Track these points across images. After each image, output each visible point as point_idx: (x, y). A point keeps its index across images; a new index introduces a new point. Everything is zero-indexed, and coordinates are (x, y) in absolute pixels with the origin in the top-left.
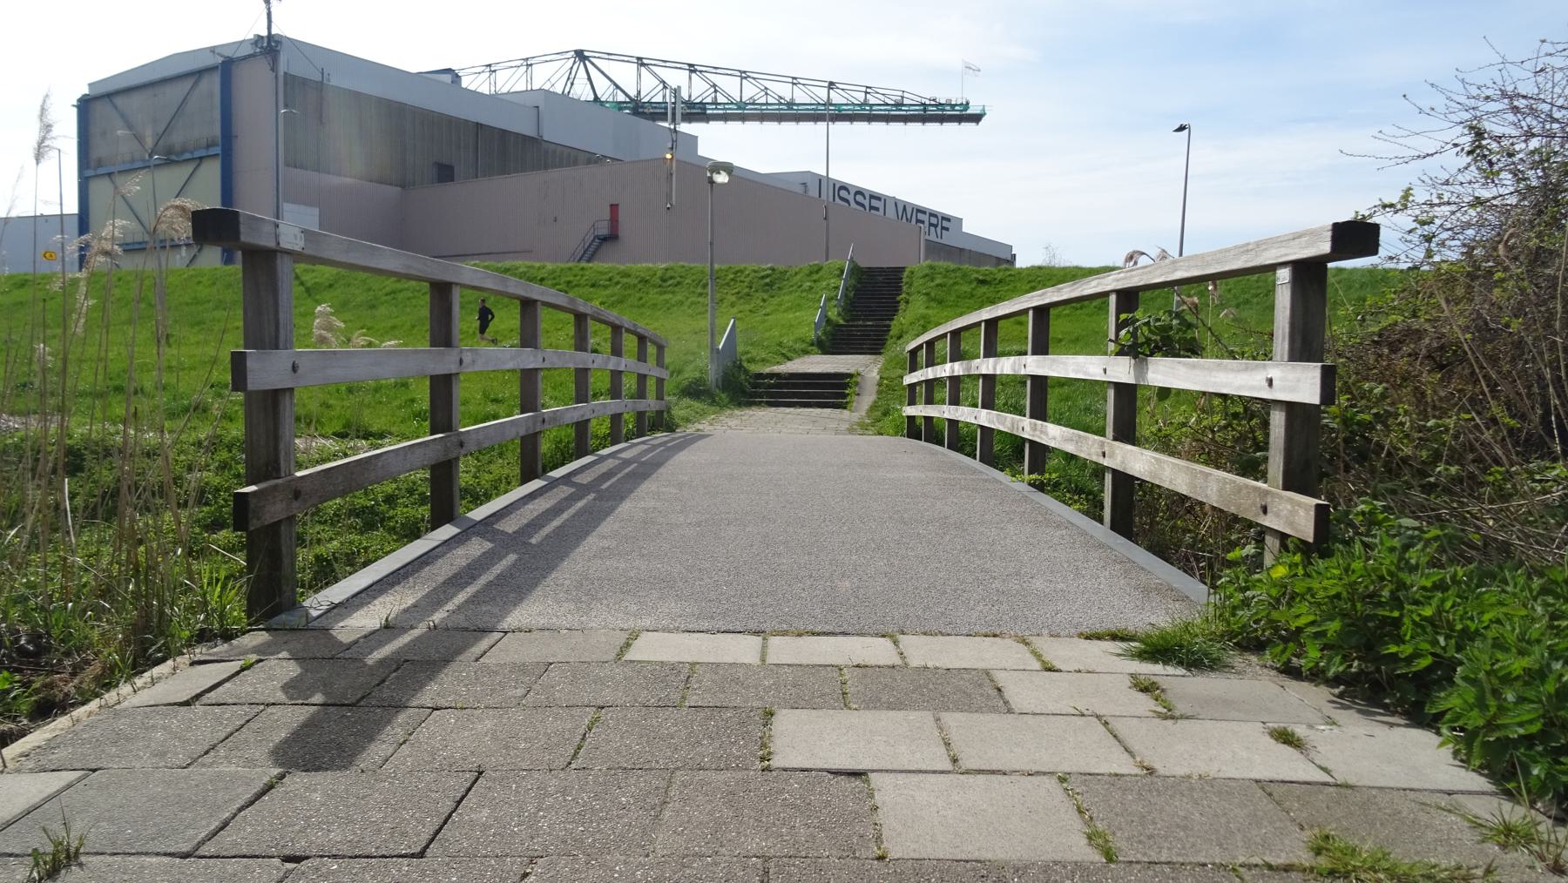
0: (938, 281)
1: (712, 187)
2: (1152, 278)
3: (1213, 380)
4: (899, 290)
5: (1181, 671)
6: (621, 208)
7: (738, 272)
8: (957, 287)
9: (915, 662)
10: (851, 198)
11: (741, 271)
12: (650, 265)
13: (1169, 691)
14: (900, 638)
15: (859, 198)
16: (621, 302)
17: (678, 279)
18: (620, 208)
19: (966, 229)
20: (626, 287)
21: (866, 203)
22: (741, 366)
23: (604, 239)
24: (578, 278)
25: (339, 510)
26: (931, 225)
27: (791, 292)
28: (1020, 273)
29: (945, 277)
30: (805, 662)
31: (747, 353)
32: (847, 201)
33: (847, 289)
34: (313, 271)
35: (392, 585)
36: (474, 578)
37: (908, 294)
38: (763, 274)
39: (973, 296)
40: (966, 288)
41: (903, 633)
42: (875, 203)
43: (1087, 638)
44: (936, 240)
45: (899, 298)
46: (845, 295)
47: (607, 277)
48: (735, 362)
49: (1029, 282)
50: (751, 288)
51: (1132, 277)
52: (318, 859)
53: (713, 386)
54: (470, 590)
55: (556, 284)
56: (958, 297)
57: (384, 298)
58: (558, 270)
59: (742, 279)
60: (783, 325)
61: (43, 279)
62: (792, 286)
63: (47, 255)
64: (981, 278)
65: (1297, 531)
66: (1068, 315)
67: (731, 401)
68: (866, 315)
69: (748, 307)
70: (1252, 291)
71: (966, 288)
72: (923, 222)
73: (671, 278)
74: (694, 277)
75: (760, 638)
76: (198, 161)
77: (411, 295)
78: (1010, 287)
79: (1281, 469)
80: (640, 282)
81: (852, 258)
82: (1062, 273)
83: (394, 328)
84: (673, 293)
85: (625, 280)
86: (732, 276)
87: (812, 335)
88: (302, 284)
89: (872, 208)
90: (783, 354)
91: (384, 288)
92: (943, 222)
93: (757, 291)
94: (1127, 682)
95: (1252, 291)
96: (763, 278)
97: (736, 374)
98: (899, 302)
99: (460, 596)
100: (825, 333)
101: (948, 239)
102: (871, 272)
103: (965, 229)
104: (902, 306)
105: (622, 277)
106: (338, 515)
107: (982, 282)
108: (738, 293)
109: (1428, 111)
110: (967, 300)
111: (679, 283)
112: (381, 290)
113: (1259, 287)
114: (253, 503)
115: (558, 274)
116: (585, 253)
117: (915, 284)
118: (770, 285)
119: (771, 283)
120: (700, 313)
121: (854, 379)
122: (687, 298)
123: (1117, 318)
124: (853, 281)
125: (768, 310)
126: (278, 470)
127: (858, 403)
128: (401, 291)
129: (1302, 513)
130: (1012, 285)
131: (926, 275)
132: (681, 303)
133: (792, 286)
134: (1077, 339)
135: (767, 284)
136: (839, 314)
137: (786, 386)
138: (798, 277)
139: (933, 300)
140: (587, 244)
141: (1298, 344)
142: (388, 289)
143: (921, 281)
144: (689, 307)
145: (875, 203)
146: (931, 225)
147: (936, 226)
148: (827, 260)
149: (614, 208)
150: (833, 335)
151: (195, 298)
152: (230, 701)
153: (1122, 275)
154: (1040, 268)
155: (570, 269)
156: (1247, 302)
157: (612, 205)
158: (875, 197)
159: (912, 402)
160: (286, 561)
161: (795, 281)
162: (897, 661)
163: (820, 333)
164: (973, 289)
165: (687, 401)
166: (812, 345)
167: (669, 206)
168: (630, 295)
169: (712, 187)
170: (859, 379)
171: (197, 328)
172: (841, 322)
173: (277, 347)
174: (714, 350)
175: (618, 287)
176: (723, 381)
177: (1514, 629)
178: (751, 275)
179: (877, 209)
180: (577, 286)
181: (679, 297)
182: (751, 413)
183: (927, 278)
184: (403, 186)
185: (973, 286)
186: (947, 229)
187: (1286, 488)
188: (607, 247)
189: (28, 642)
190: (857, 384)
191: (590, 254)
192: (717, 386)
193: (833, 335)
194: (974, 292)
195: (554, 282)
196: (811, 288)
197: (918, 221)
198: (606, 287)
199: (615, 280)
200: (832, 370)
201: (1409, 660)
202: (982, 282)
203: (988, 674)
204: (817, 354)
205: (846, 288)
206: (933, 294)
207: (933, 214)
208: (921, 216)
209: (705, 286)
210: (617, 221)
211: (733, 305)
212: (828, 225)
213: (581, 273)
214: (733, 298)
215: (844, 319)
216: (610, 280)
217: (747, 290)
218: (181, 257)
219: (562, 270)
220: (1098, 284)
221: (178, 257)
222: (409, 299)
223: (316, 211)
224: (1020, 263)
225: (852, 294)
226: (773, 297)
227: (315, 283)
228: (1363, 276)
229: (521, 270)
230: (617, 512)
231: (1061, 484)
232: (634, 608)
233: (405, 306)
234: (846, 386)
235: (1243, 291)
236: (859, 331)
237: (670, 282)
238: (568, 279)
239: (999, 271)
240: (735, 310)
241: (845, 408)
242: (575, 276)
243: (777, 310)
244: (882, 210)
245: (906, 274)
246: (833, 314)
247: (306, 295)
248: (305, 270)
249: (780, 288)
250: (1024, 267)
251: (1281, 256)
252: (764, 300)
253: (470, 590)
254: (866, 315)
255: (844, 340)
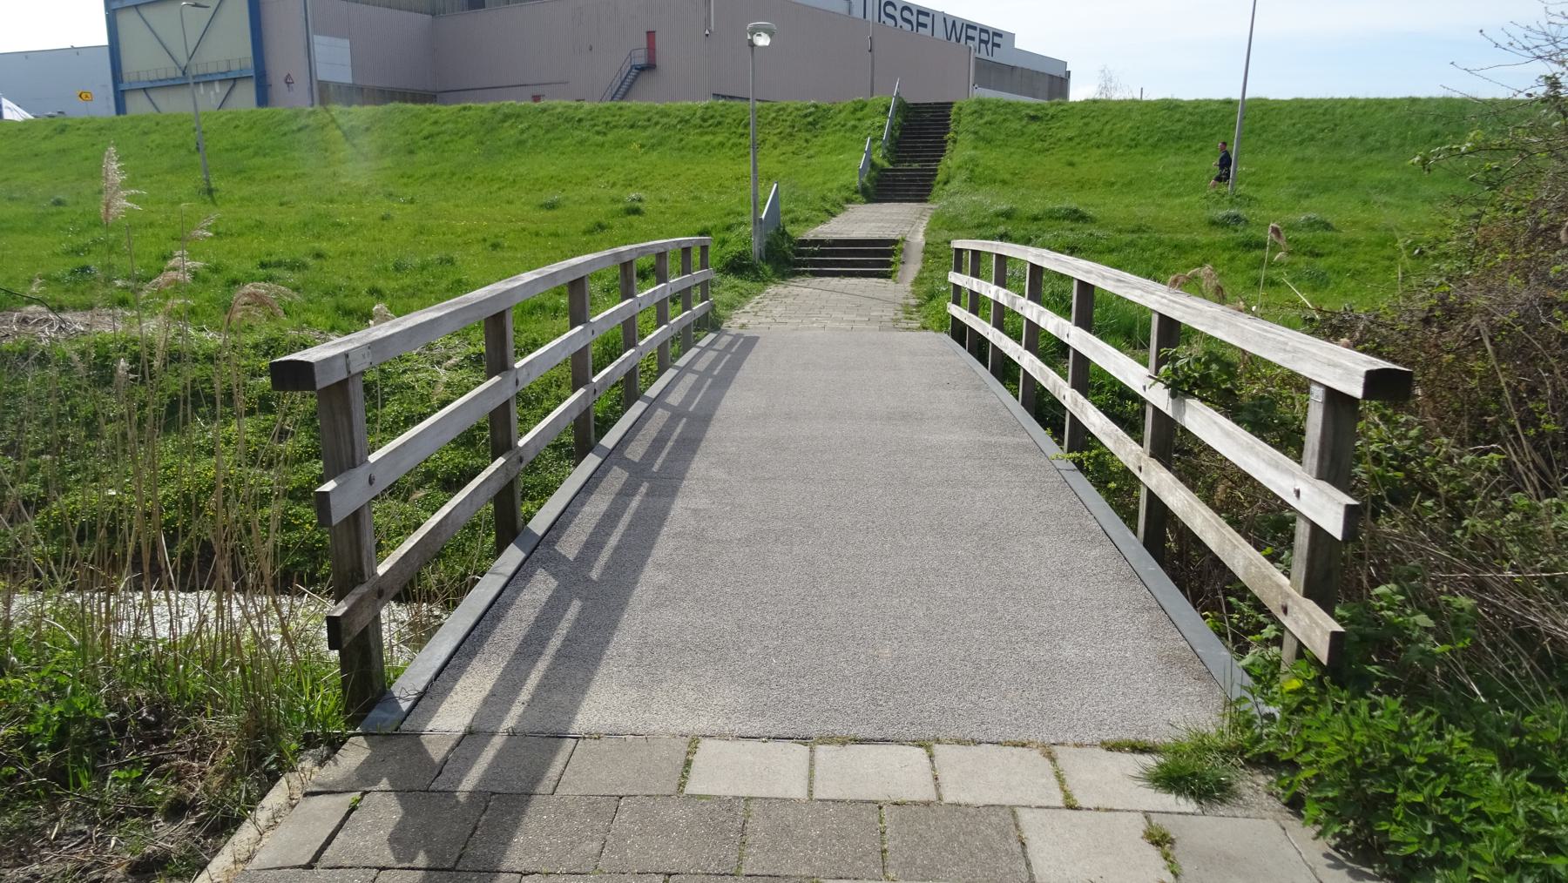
0: (986, 119)
1: (753, 51)
2: (1195, 322)
3: (1245, 458)
4: (946, 128)
5: (1189, 805)
6: (657, 36)
7: (780, 110)
8: (1008, 124)
9: (949, 797)
10: (897, 14)
11: (783, 109)
12: (690, 103)
13: (1178, 845)
14: (937, 748)
15: (906, 14)
16: (660, 144)
17: (719, 119)
18: (657, 34)
19: (1018, 45)
20: (666, 127)
21: (914, 19)
22: (784, 233)
23: (642, 69)
24: (617, 118)
25: (397, 417)
26: (981, 41)
27: (834, 132)
28: (1073, 108)
29: (995, 113)
30: (849, 796)
31: (791, 211)
32: (892, 17)
33: (892, 128)
34: (349, 113)
35: (471, 655)
36: (543, 642)
37: (956, 132)
38: (805, 112)
39: (1023, 134)
40: (1016, 125)
41: (938, 741)
42: (922, 19)
43: (1109, 749)
44: (985, 57)
45: (946, 138)
46: (891, 135)
47: (646, 117)
48: (778, 229)
49: (1083, 118)
50: (794, 127)
51: (1174, 308)
52: (415, 786)
53: (757, 257)
54: (542, 665)
55: (595, 125)
56: (1007, 135)
57: (421, 143)
58: (597, 110)
59: (784, 117)
60: (826, 170)
61: (82, 124)
62: (835, 125)
63: (83, 96)
64: (1032, 113)
65: (1313, 646)
66: (1122, 155)
67: (776, 271)
68: (911, 157)
69: (791, 149)
70: (1319, 126)
71: (1016, 125)
72: (973, 39)
73: (712, 117)
74: (734, 116)
75: (807, 748)
76: (231, 83)
77: (448, 138)
78: (1062, 123)
79: (1304, 573)
80: (680, 122)
81: (898, 93)
82: (1118, 107)
83: (434, 176)
84: (714, 134)
85: (665, 120)
86: (774, 115)
87: (857, 182)
88: (339, 127)
89: (919, 24)
90: (827, 211)
91: (421, 131)
92: (993, 38)
93: (800, 130)
94: (1140, 825)
95: (1319, 126)
96: (806, 116)
97: (780, 243)
98: (946, 142)
99: (532, 676)
100: (869, 179)
101: (999, 56)
102: (917, 109)
103: (1017, 45)
104: (950, 146)
105: (662, 117)
106: (397, 423)
107: (1034, 118)
108: (780, 133)
109: (1506, 46)
110: (1017, 139)
111: (720, 123)
112: (418, 134)
113: (1325, 121)
114: (344, 624)
115: (596, 114)
116: (622, 83)
117: (964, 122)
118: (813, 124)
119: (815, 121)
120: (741, 156)
121: (899, 246)
122: (729, 139)
123: (1158, 353)
124: (899, 119)
125: (812, 152)
126: (362, 575)
127: (903, 272)
128: (438, 134)
129: (1318, 632)
130: (1065, 121)
131: (975, 112)
132: (722, 144)
133: (835, 125)
134: (1131, 183)
135: (810, 123)
136: (884, 157)
137: (831, 253)
138: (843, 115)
139: (983, 139)
140: (623, 76)
141: (1327, 463)
142: (425, 133)
143: (970, 118)
144: (731, 149)
145: (922, 19)
146: (981, 41)
147: (986, 43)
148: (872, 96)
149: (651, 35)
150: (878, 181)
151: (235, 144)
152: (348, 863)
153: (1165, 301)
154: (1095, 101)
155: (608, 108)
156: (1312, 138)
157: (648, 33)
158: (922, 12)
159: (959, 269)
160: (375, 653)
161: (837, 121)
162: (933, 797)
163: (864, 180)
164: (1024, 127)
165: (732, 280)
166: (857, 192)
167: (707, 32)
168: (669, 136)
169: (753, 51)
170: (904, 245)
171: (238, 177)
172: (887, 165)
173: (354, 466)
174: (758, 221)
175: (658, 127)
176: (767, 251)
177: (1492, 846)
178: (794, 114)
179: (925, 26)
180: (615, 127)
181: (720, 139)
182: (796, 290)
183: (976, 115)
184: (433, 15)
185: (1024, 123)
186: (998, 46)
187: (1307, 595)
188: (645, 77)
189: (149, 713)
190: (902, 251)
191: (624, 90)
192: (761, 258)
193: (878, 181)
194: (1025, 130)
195: (592, 123)
196: (855, 127)
197: (968, 38)
198: (645, 128)
199: (654, 121)
200: (876, 235)
201: (1398, 845)
202: (1034, 118)
203: (1014, 814)
204: (860, 202)
205: (892, 127)
206: (981, 133)
207: (984, 30)
208: (971, 32)
209: (746, 126)
210: (654, 50)
211: (775, 146)
212: (873, 57)
213: (619, 113)
214: (776, 139)
215: (889, 161)
216: (649, 120)
217: (789, 130)
218: (216, 94)
219: (600, 109)
220: (1142, 296)
221: (212, 93)
222: (446, 143)
223: (347, 43)
224: (1078, 92)
225: (897, 134)
226: (816, 137)
227: (352, 127)
228: (1438, 107)
229: (559, 110)
230: (669, 517)
231: (1104, 386)
232: (691, 696)
233: (443, 151)
234: (891, 253)
235: (1308, 126)
236: (903, 176)
237: (710, 122)
238: (607, 120)
239: (1052, 105)
240: (777, 152)
241: (890, 277)
242: (614, 116)
243: (820, 152)
244: (930, 26)
245: (954, 109)
246: (878, 157)
247: (343, 139)
248: (341, 112)
249: (823, 128)
250: (1078, 100)
251: (1316, 375)
252: (807, 141)
253: (542, 665)
254: (911, 157)
255: (888, 185)
